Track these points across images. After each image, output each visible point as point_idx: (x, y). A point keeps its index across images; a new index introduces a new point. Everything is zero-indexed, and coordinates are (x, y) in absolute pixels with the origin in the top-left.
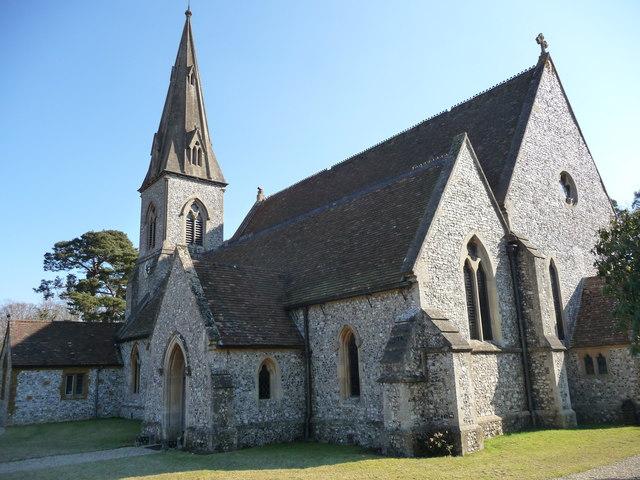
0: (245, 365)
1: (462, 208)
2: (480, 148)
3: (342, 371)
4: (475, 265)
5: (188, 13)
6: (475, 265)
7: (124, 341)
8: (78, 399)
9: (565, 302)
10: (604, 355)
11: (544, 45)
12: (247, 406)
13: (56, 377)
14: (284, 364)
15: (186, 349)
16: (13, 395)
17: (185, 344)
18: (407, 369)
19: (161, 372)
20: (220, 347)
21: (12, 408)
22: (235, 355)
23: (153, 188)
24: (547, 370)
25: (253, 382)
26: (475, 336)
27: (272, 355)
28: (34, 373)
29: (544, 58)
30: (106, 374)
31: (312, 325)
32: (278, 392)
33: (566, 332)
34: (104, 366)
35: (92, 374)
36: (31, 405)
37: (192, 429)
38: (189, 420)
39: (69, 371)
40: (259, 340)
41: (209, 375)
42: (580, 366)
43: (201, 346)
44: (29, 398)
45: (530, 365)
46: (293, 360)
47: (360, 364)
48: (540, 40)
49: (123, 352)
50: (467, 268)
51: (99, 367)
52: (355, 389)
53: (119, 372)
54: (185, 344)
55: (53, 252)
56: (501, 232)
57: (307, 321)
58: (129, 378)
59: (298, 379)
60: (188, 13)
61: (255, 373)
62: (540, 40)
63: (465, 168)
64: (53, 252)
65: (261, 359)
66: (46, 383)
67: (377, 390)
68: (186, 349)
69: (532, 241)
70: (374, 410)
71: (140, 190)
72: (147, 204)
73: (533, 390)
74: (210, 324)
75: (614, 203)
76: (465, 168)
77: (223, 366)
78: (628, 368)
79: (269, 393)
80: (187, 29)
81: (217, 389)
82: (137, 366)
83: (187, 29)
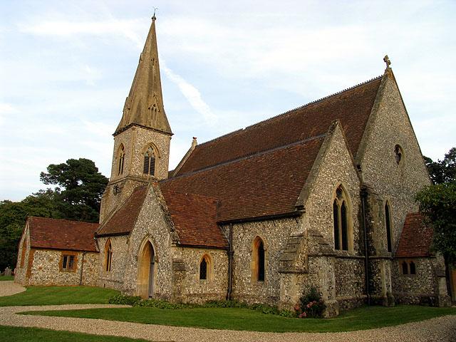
0: (193, 257)
1: (332, 173)
2: (346, 126)
3: (254, 264)
4: (340, 203)
5: (154, 18)
6: (340, 203)
7: (100, 236)
8: (70, 272)
9: (394, 240)
10: (414, 262)
11: (388, 63)
12: (193, 286)
13: (57, 256)
14: (217, 259)
15: (155, 244)
16: (30, 265)
17: (154, 241)
18: (297, 265)
19: (137, 258)
20: (178, 246)
21: (29, 274)
22: (187, 251)
23: (123, 134)
24: (379, 270)
25: (197, 269)
26: (337, 247)
27: (210, 252)
28: (44, 253)
29: (389, 74)
30: (88, 257)
31: (235, 235)
32: (211, 275)
33: (393, 247)
34: (88, 252)
35: (80, 256)
36: (41, 272)
37: (158, 294)
38: (156, 289)
39: (66, 253)
40: (202, 242)
41: (171, 262)
42: (400, 270)
43: (167, 244)
44: (40, 268)
45: (267, 220)
46: (222, 256)
47: (265, 261)
48: (386, 59)
49: (99, 243)
50: (335, 206)
51: (85, 252)
52: (261, 276)
53: (97, 256)
54: (154, 241)
55: (47, 172)
56: (358, 183)
57: (231, 233)
58: (104, 261)
59: (224, 268)
60: (154, 18)
61: (198, 263)
62: (386, 59)
63: (337, 144)
64: (47, 172)
65: (202, 254)
66: (52, 260)
67: (275, 278)
68: (155, 244)
69: (376, 188)
70: (272, 290)
71: (114, 135)
72: (119, 144)
73: (370, 282)
74: (173, 231)
75: (428, 160)
76: (337, 144)
77: (180, 257)
78: (428, 271)
79: (205, 276)
80: (153, 25)
81: (176, 271)
82: (109, 254)
83: (153, 25)
